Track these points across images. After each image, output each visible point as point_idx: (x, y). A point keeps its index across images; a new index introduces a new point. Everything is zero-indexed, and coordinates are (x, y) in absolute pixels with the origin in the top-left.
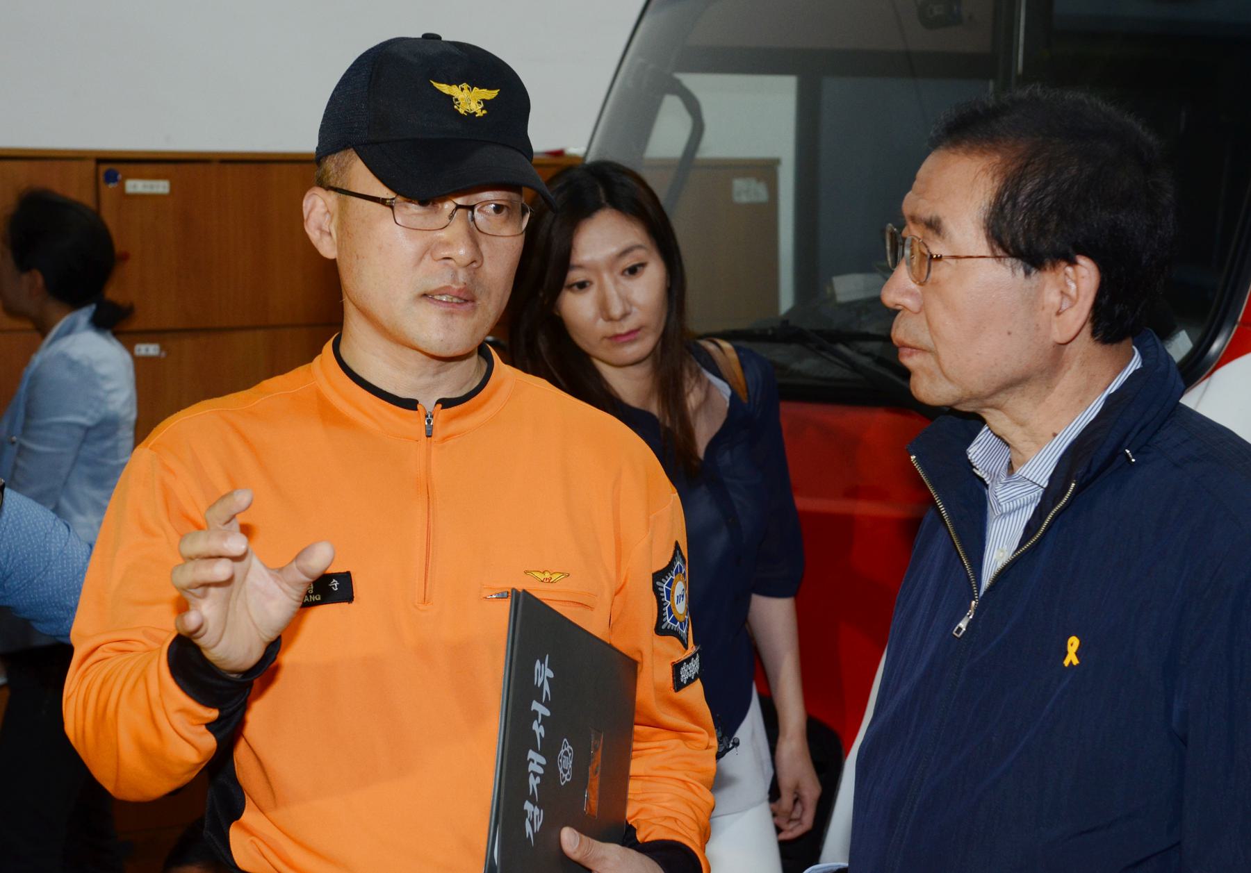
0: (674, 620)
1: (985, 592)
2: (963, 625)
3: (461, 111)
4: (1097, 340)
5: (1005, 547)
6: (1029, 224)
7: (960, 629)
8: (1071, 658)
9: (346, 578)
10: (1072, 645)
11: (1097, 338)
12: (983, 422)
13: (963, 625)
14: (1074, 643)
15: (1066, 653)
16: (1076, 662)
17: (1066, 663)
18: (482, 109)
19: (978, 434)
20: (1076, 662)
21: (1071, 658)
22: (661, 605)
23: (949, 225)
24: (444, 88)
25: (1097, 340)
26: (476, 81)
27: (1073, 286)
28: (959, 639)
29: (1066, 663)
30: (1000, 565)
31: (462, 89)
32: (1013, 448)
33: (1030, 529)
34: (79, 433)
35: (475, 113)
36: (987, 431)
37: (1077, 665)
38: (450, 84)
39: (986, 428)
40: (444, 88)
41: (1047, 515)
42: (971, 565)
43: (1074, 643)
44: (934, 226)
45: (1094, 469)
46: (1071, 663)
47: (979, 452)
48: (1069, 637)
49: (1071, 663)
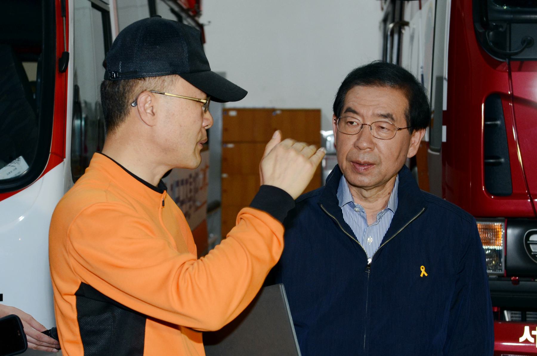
15: (421, 272)
17: (422, 275)
20: (426, 275)
29: (422, 275)
37: (427, 276)
46: (424, 274)
49: (424, 274)
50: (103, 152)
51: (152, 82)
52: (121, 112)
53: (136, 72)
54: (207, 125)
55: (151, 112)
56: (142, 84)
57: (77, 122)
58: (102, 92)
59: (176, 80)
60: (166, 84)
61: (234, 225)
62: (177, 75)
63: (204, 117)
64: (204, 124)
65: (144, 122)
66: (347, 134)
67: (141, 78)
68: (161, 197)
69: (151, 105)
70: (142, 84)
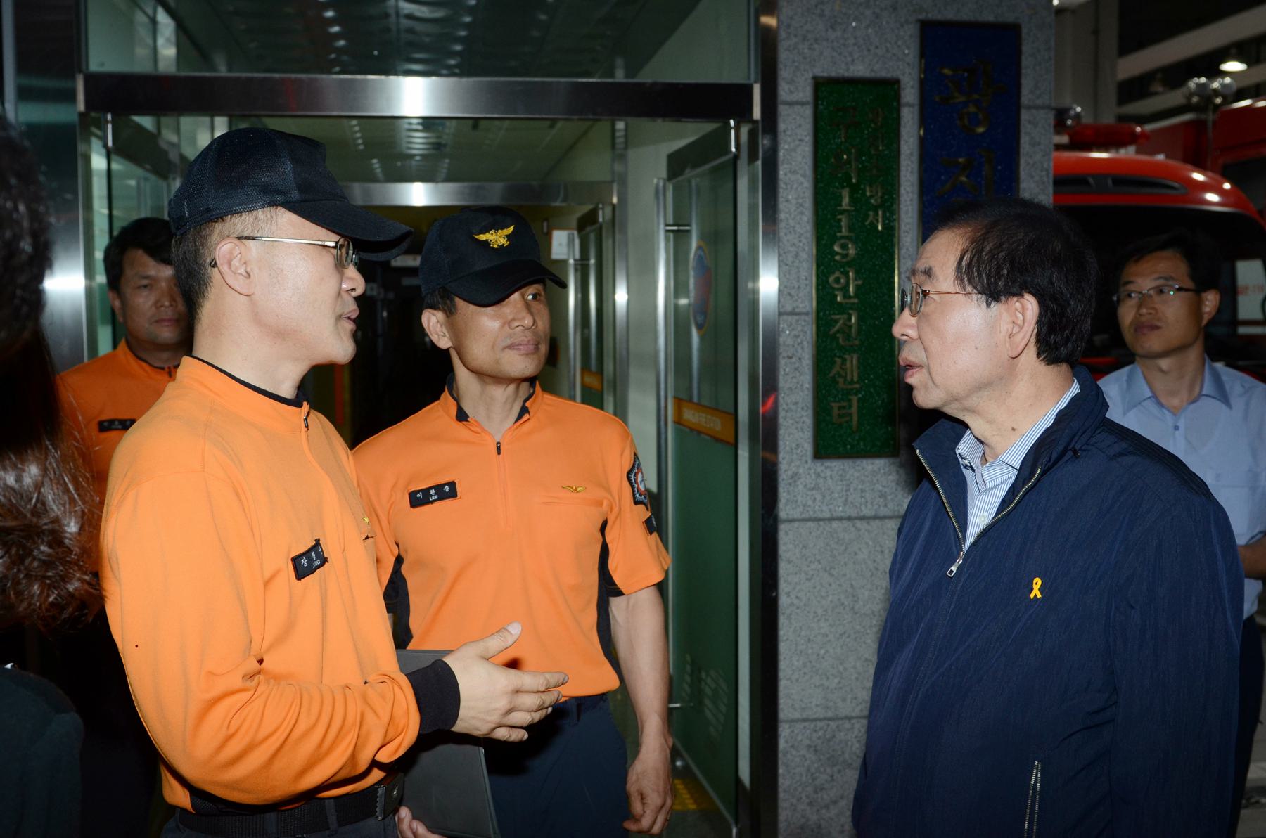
0: (640, 495)
1: (970, 547)
2: (954, 568)
3: (495, 246)
4: (1041, 361)
5: (985, 514)
6: (990, 270)
7: (952, 571)
8: (1036, 592)
9: (452, 484)
10: (1036, 583)
11: (1041, 359)
12: (966, 426)
13: (954, 568)
14: (1037, 583)
15: (1032, 589)
16: (1039, 596)
17: (1032, 596)
18: (507, 241)
19: (963, 436)
20: (1039, 596)
21: (1036, 592)
22: (632, 487)
23: (937, 270)
24: (482, 237)
25: (1041, 361)
26: (497, 226)
27: (1020, 316)
28: (952, 578)
29: (1032, 596)
30: (982, 527)
31: (492, 234)
32: (986, 445)
33: (1004, 503)
34: (471, 122)
35: (503, 244)
36: (969, 435)
38: (484, 233)
39: (969, 432)
40: (482, 237)
41: (1019, 492)
42: (960, 527)
43: (1037, 583)
44: (928, 273)
45: (1053, 460)
46: (1036, 595)
47: (965, 447)
48: (1033, 579)
49: (1036, 595)
50: (195, 354)
51: (241, 223)
52: (200, 284)
53: (208, 210)
54: (351, 288)
55: (245, 274)
56: (220, 227)
57: (588, 379)
58: (768, 455)
59: (277, 215)
60: (261, 223)
61: (388, 612)
62: (279, 208)
63: (346, 275)
64: (344, 286)
65: (230, 287)
66: (284, 742)
67: (217, 218)
68: (301, 412)
69: (243, 261)
70: (220, 227)
